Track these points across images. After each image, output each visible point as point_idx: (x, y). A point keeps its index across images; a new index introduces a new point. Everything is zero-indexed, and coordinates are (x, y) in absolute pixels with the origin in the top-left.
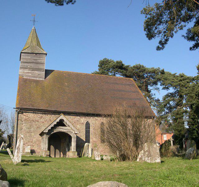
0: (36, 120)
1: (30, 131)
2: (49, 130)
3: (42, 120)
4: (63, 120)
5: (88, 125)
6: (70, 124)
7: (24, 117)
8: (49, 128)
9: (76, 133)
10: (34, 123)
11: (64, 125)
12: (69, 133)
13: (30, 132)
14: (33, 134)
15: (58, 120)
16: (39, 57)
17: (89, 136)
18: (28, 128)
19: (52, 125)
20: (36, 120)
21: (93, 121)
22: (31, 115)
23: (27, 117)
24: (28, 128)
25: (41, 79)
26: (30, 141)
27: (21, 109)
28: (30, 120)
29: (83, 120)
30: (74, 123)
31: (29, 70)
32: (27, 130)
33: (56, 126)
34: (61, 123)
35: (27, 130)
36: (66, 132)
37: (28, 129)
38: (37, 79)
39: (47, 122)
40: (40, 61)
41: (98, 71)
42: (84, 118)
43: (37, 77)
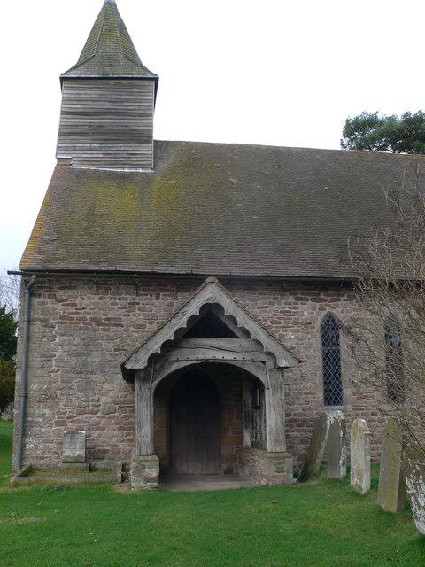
0: (108, 319)
1: (85, 365)
2: (153, 359)
3: (136, 317)
4: (218, 307)
5: (331, 329)
6: (252, 327)
7: (59, 307)
8: (155, 346)
9: (283, 363)
10: (100, 332)
11: (226, 333)
12: (250, 368)
13: (82, 370)
14: (97, 377)
15: (194, 309)
16: (131, 94)
17: (337, 374)
18: (78, 355)
19: (168, 334)
20: (108, 319)
21: (343, 310)
22: (88, 301)
23: (71, 309)
24: (78, 355)
25: (140, 171)
26: (80, 405)
27: (42, 274)
28: (82, 319)
29: (311, 311)
30: (273, 323)
31: (95, 141)
32: (74, 361)
33: (184, 336)
34: (210, 323)
35: (74, 361)
36: (234, 363)
37: (75, 359)
38: (126, 170)
39: (151, 323)
40: (132, 106)
41: (173, 120)
42: (313, 300)
43: (124, 164)
